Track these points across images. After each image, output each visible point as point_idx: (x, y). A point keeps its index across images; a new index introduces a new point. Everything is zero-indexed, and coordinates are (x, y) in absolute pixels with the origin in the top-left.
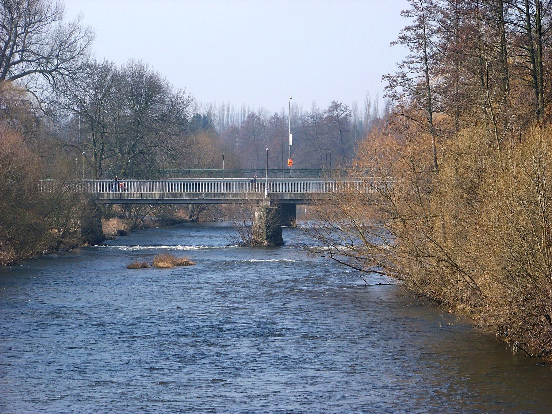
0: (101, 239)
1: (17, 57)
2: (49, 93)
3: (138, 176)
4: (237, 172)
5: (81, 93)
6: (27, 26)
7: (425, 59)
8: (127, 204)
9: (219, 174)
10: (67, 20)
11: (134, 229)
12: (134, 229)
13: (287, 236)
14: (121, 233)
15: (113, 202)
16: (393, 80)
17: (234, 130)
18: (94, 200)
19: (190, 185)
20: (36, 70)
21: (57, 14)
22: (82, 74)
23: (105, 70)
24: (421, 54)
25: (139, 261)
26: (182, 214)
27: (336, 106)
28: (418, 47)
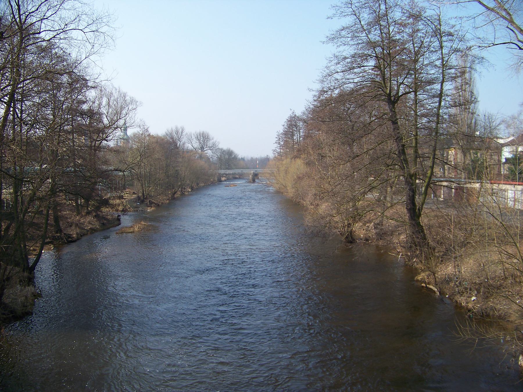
0: (221, 181)
1: (205, 147)
2: (211, 154)
3: (228, 169)
4: (248, 168)
5: (217, 154)
6: (207, 141)
7: (280, 147)
8: (226, 175)
9: (244, 169)
10: (214, 140)
11: (228, 179)
12: (228, 179)
13: (256, 180)
14: (225, 180)
15: (223, 174)
16: (274, 151)
17: (248, 161)
18: (219, 174)
19: (242, 171)
20: (414, 111)
21: (213, 139)
22: (218, 150)
23: (222, 149)
24: (279, 145)
25: (227, 185)
26: (237, 176)
27: (267, 156)
28: (279, 144)
